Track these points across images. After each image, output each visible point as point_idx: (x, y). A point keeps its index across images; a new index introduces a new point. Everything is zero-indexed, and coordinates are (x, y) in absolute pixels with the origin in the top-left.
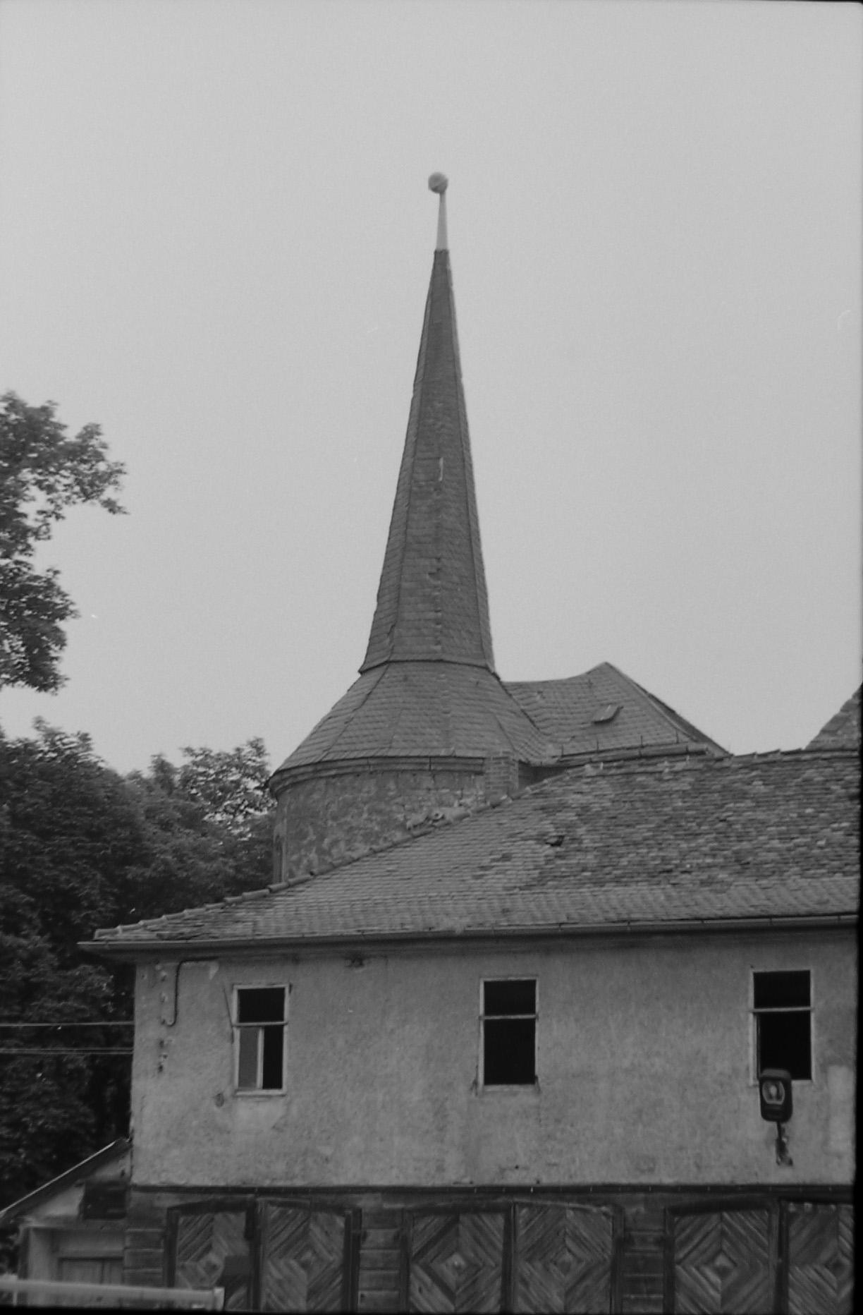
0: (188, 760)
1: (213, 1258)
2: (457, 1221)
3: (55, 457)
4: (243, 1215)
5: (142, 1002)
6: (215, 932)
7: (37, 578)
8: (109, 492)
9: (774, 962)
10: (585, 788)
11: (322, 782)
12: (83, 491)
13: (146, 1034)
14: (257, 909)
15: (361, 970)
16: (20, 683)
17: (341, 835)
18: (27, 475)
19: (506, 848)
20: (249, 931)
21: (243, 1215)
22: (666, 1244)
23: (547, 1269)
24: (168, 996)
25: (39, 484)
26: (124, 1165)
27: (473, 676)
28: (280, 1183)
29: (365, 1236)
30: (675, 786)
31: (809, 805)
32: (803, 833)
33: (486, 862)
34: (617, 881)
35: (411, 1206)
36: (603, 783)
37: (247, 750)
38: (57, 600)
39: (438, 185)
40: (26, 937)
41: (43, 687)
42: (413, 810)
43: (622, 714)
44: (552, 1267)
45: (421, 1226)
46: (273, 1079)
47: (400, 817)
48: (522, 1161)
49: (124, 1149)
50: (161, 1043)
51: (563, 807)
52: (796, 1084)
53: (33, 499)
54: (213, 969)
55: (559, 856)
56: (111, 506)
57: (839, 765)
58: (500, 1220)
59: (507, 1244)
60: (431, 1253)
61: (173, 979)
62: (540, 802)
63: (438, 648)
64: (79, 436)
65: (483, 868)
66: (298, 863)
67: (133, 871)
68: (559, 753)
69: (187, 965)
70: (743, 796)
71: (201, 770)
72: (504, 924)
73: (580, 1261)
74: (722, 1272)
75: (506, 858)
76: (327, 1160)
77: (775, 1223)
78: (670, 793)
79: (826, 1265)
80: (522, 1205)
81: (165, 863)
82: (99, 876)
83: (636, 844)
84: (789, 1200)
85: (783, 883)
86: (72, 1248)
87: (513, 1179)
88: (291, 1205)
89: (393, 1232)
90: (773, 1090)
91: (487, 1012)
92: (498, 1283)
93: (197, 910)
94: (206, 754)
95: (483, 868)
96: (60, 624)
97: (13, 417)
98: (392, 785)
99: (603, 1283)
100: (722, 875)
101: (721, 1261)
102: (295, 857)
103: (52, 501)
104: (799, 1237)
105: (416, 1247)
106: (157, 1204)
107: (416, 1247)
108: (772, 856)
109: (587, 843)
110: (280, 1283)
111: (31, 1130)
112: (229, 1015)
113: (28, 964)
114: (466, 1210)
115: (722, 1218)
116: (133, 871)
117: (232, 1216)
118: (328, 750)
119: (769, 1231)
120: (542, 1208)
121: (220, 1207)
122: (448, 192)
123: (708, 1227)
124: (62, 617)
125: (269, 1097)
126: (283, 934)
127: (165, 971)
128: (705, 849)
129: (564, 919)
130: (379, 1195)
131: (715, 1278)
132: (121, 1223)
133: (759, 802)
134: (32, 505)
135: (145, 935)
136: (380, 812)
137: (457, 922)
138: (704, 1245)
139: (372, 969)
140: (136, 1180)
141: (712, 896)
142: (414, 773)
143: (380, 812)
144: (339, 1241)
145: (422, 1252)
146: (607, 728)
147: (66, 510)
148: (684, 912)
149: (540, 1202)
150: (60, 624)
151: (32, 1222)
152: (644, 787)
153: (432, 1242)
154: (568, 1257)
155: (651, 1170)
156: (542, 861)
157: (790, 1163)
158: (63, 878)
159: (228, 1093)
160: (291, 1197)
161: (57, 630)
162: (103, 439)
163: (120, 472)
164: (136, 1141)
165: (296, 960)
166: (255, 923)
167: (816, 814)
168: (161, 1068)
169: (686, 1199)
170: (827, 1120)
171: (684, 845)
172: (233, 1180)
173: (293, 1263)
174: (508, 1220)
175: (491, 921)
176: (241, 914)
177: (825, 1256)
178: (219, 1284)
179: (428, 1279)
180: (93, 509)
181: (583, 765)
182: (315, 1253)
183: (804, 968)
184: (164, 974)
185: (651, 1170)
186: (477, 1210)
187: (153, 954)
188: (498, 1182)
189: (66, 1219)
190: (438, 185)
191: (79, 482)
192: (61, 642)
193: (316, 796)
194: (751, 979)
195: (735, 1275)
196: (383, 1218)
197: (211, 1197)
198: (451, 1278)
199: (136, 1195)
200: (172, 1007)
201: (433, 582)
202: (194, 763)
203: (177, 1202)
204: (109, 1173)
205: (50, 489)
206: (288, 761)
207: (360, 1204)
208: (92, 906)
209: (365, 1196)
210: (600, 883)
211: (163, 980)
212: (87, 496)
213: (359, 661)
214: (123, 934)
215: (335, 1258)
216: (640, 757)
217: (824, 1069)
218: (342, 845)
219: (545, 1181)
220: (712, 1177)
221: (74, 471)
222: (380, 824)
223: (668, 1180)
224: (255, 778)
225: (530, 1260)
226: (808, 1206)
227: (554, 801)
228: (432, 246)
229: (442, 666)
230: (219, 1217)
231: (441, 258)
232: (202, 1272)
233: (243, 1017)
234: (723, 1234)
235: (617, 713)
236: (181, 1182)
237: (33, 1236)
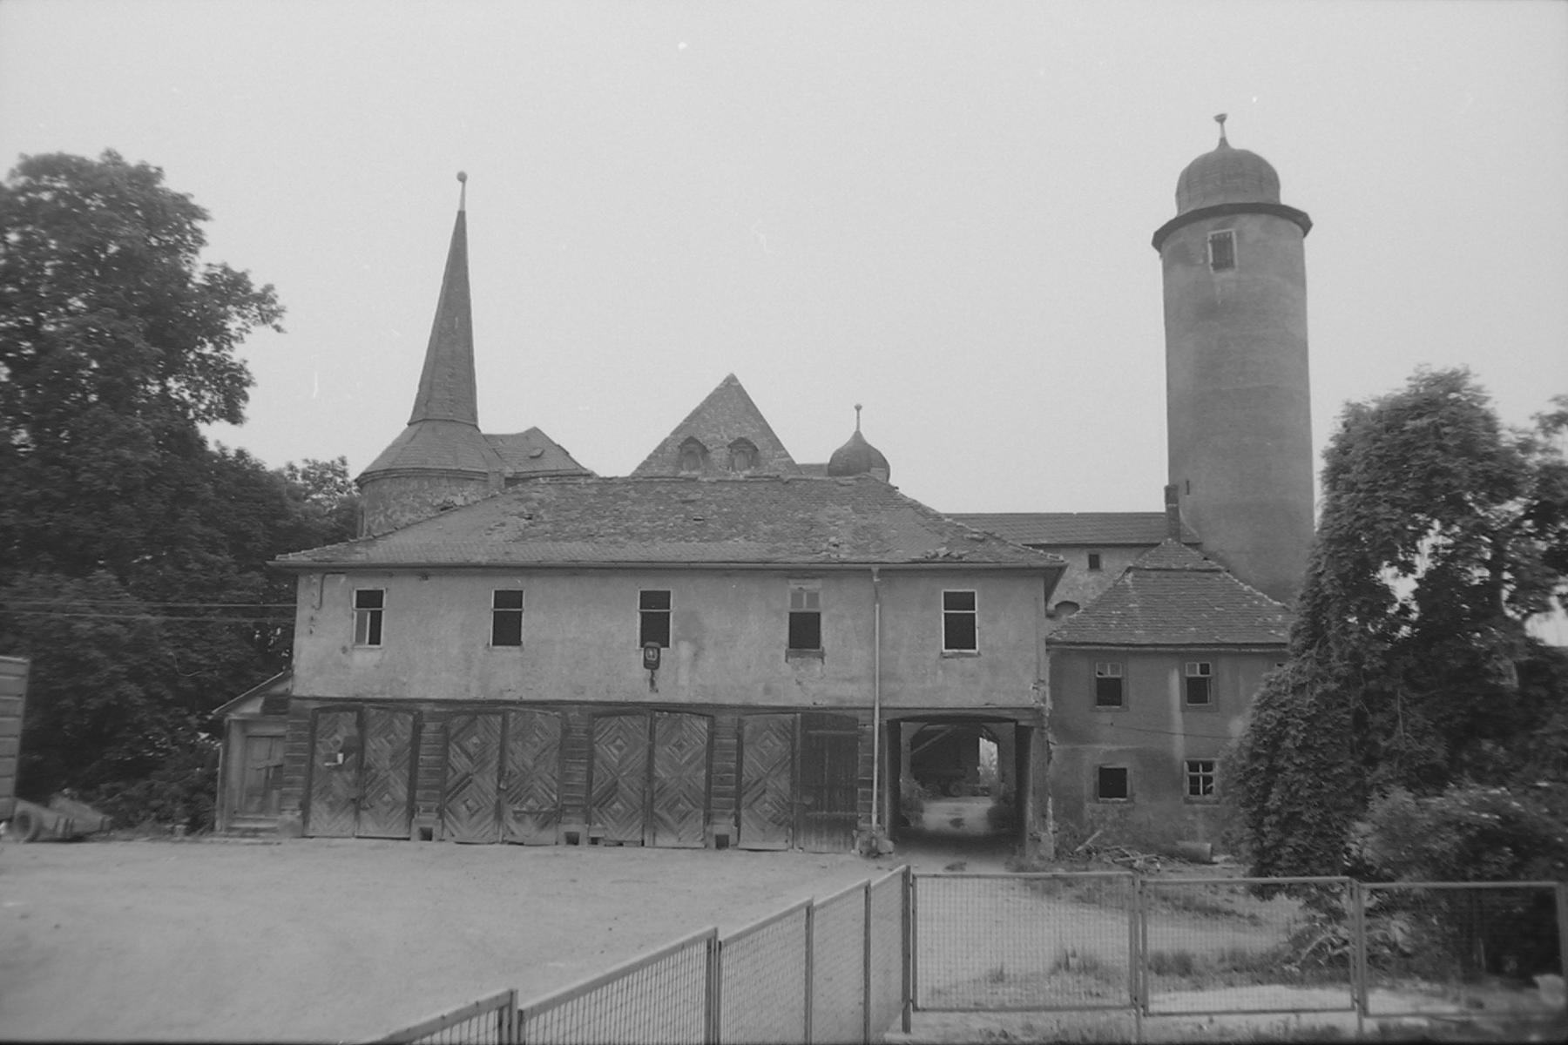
0: (305, 466)
1: (338, 737)
2: (476, 718)
3: (248, 299)
4: (355, 714)
5: (302, 595)
6: (345, 558)
7: (234, 364)
8: (277, 321)
9: (651, 585)
10: (541, 490)
11: (388, 481)
12: (263, 319)
13: (303, 614)
14: (367, 546)
15: (426, 582)
16: (222, 420)
17: (397, 508)
18: (230, 308)
19: (503, 520)
20: (364, 558)
21: (355, 714)
22: (589, 732)
23: (524, 745)
24: (317, 593)
25: (238, 313)
26: (289, 685)
27: (469, 430)
28: (378, 696)
29: (424, 725)
30: (587, 491)
31: (661, 504)
32: (660, 519)
33: (492, 526)
34: (565, 539)
35: (451, 710)
36: (549, 487)
37: (337, 462)
38: (245, 376)
39: (462, 178)
40: (221, 556)
41: (234, 423)
42: (437, 497)
43: (546, 453)
44: (528, 745)
45: (456, 721)
46: (375, 639)
47: (430, 500)
48: (513, 687)
49: (289, 676)
50: (312, 619)
51: (531, 499)
52: (662, 649)
53: (236, 320)
54: (343, 579)
55: (531, 525)
56: (278, 329)
57: (674, 485)
58: (500, 719)
59: (503, 731)
60: (461, 735)
61: (319, 584)
62: (517, 496)
63: (451, 414)
64: (263, 290)
65: (491, 530)
66: (373, 522)
67: (281, 523)
68: (513, 471)
69: (328, 576)
70: (626, 498)
71: (312, 471)
72: (507, 560)
73: (542, 741)
74: (620, 748)
75: (503, 524)
76: (404, 684)
77: (648, 723)
78: (586, 495)
79: (674, 745)
80: (513, 711)
81: (298, 518)
82: (261, 524)
83: (572, 520)
84: (658, 710)
85: (654, 544)
86: (255, 730)
87: (507, 696)
88: (382, 708)
89: (440, 724)
90: (651, 653)
91: (495, 607)
92: (498, 752)
93: (334, 546)
94: (315, 463)
95: (491, 530)
96: (246, 389)
97: (225, 277)
98: (426, 483)
99: (555, 753)
100: (621, 539)
101: (619, 742)
102: (371, 519)
103: (244, 323)
104: (661, 729)
105: (453, 732)
106: (307, 707)
107: (453, 732)
108: (646, 530)
109: (546, 519)
110: (375, 751)
111: (222, 660)
112: (352, 604)
113: (223, 570)
114: (480, 713)
115: (620, 720)
116: (281, 523)
117: (349, 714)
118: (393, 463)
119: (645, 727)
120: (523, 713)
121: (343, 709)
122: (468, 182)
123: (612, 724)
124: (247, 385)
125: (372, 649)
126: (385, 561)
127: (316, 579)
128: (610, 525)
129: (540, 559)
130: (432, 704)
131: (616, 752)
132: (284, 717)
133: (634, 502)
134: (233, 325)
135: (305, 559)
136: (420, 497)
137: (483, 559)
138: (610, 733)
139: (433, 580)
140: (294, 694)
141: (617, 549)
142: (438, 478)
143: (420, 497)
144: (409, 728)
145: (456, 735)
146: (537, 460)
147: (253, 328)
148: (605, 558)
149: (521, 709)
150: (246, 389)
151: (233, 716)
152: (571, 490)
153: (462, 730)
154: (536, 739)
155: (583, 693)
156: (522, 528)
157: (657, 691)
158: (243, 524)
159: (349, 645)
160: (385, 705)
161: (244, 392)
162: (275, 292)
163: (283, 311)
164: (296, 672)
165: (391, 575)
166: (368, 555)
167: (1510, 530)
168: (311, 632)
169: (600, 709)
170: (677, 669)
171: (598, 522)
172: (350, 694)
173: (383, 740)
174: (504, 719)
175: (501, 559)
176: (358, 549)
177: (674, 740)
178: (341, 751)
179: (458, 750)
180: (267, 330)
181: (537, 477)
182: (395, 735)
183: (666, 589)
184: (315, 580)
185: (583, 693)
186: (487, 713)
187: (310, 569)
188: (499, 698)
189: (253, 715)
190: (462, 178)
191: (261, 314)
192: (246, 398)
193: (385, 487)
194: (639, 594)
195: (625, 750)
196: (434, 717)
197: (335, 703)
198: (472, 750)
199: (294, 701)
200: (318, 599)
201: (449, 380)
202: (309, 468)
203: (318, 706)
204: (279, 689)
205: (244, 317)
206: (369, 467)
207: (422, 708)
208: (258, 541)
209: (424, 704)
210: (555, 540)
211: (314, 584)
212: (264, 321)
213: (408, 417)
214: (292, 558)
215: (407, 738)
216: (557, 476)
217: (676, 643)
218: (398, 513)
219: (525, 698)
220: (613, 698)
221: (259, 308)
222: (420, 503)
223: (592, 699)
224: (340, 476)
225: (515, 740)
226: (666, 713)
227: (524, 496)
228: (457, 208)
229: (453, 424)
230: (342, 715)
231: (461, 215)
232: (331, 745)
233: (358, 606)
234: (620, 728)
235: (542, 453)
236: (320, 695)
237: (233, 724)
